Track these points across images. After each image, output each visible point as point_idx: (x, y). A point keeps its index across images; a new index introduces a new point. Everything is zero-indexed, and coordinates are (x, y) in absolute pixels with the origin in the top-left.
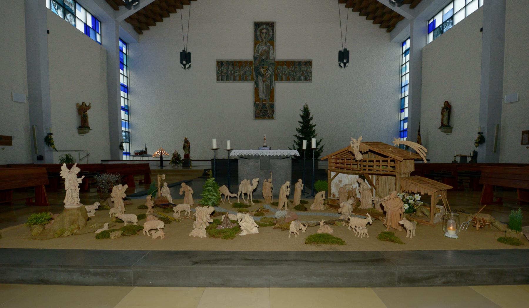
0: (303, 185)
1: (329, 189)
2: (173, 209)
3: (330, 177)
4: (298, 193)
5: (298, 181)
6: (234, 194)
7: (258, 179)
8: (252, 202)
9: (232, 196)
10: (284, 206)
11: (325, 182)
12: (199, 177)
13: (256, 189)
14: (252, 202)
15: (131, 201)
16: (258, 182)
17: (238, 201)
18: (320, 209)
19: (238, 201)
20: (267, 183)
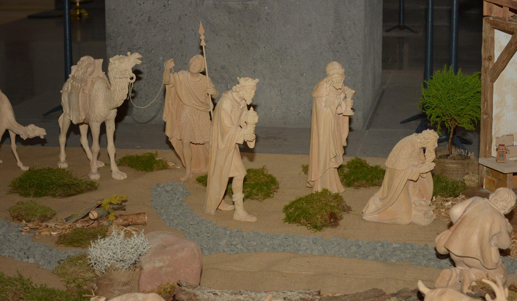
0: (350, 92)
1: (485, 117)
2: (259, 294)
3: (490, 58)
4: (321, 138)
5: (324, 75)
6: (31, 127)
7: (137, 55)
8: (114, 167)
9: (24, 137)
10: (228, 192)
11: (471, 79)
12: (30, 17)
13: (126, 103)
14: (114, 167)
15: (126, 212)
16: (137, 72)
17: (63, 156)
18: (407, 221)
19: (63, 156)
20: (182, 76)
